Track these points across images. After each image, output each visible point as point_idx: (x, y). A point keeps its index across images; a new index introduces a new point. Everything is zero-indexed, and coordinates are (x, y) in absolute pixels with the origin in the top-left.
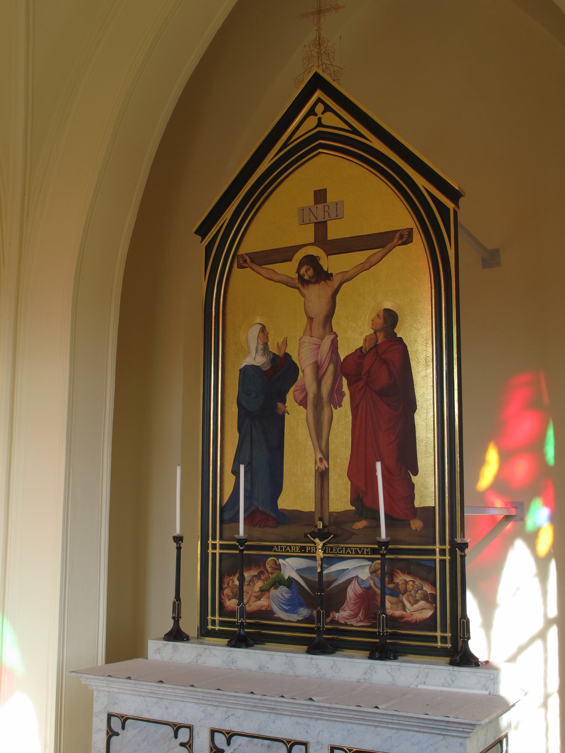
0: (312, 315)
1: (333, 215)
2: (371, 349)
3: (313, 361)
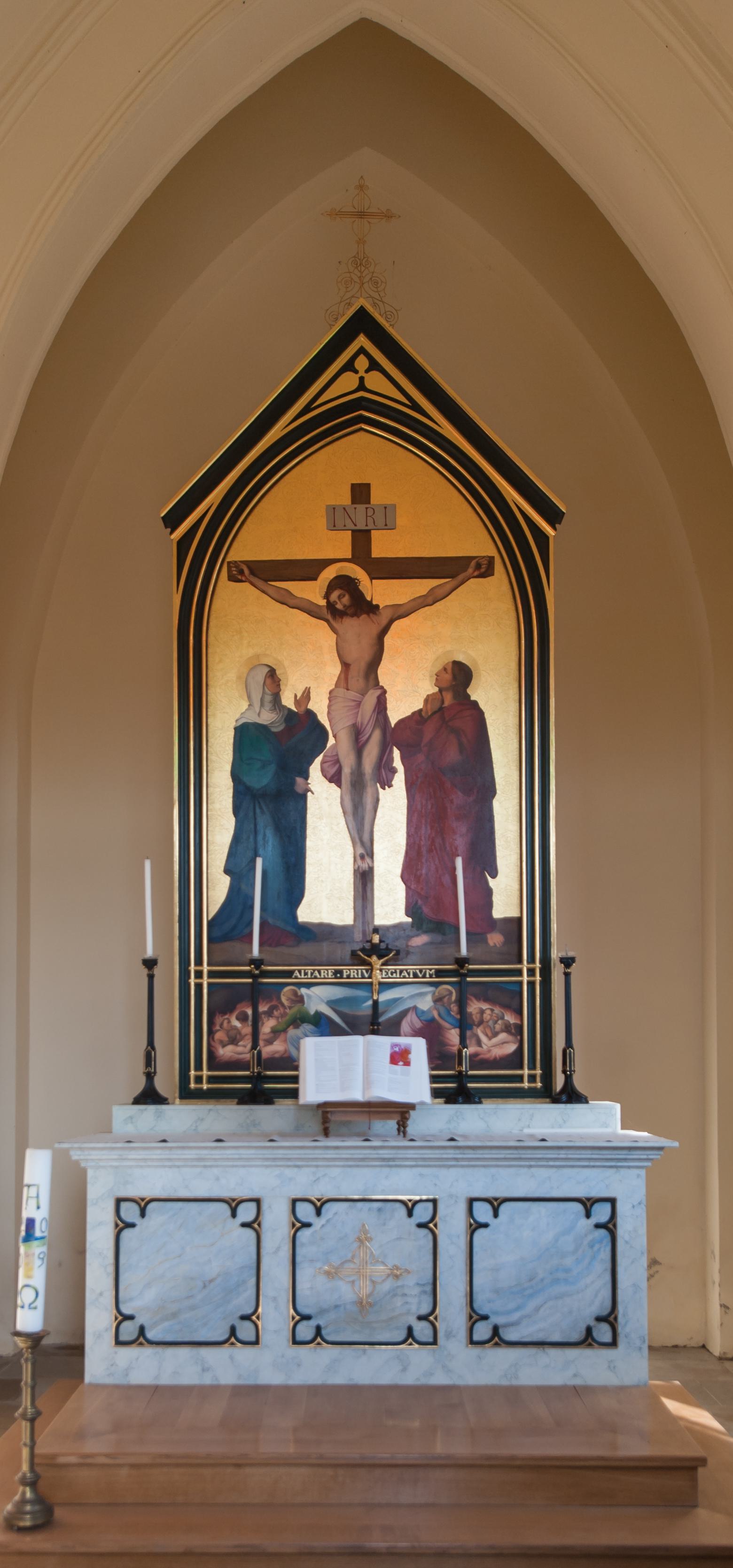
0: (349, 660)
1: (380, 522)
2: (434, 713)
3: (350, 723)
